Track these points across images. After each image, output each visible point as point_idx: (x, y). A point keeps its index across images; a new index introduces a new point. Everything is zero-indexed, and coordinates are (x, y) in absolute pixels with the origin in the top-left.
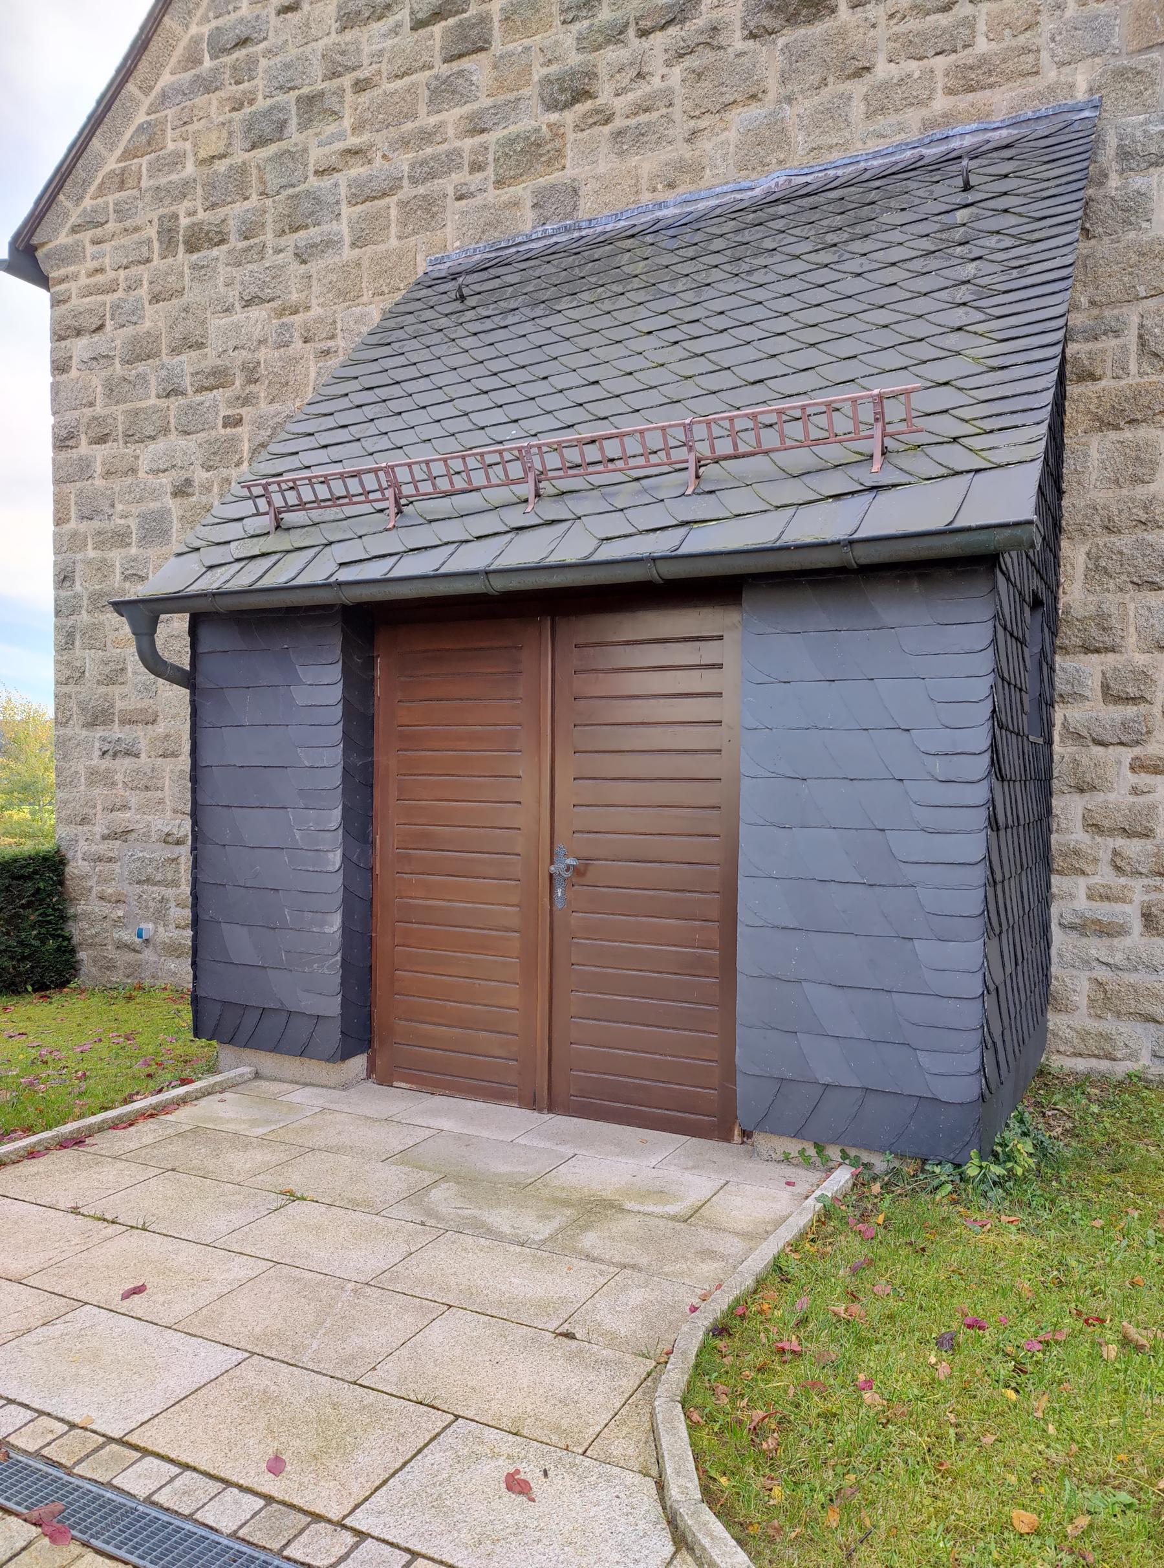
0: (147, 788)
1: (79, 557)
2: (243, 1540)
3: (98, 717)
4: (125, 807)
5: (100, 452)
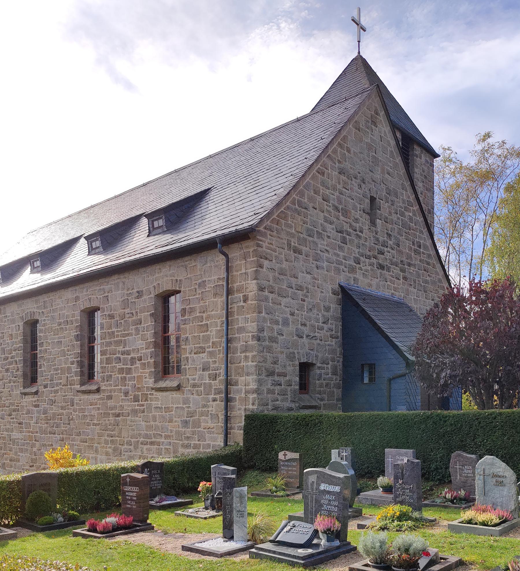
0: (284, 395)
1: (265, 325)
2: (227, 389)
3: (271, 373)
4: (278, 400)
5: (271, 296)
